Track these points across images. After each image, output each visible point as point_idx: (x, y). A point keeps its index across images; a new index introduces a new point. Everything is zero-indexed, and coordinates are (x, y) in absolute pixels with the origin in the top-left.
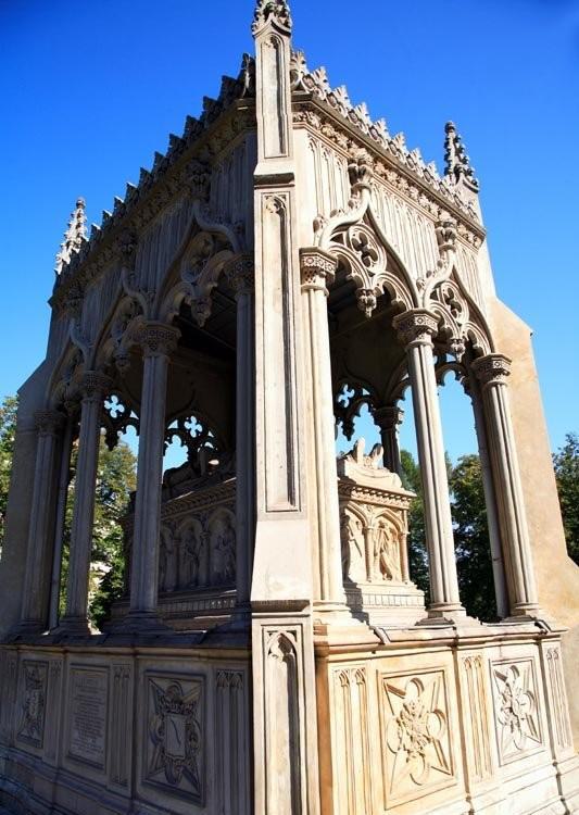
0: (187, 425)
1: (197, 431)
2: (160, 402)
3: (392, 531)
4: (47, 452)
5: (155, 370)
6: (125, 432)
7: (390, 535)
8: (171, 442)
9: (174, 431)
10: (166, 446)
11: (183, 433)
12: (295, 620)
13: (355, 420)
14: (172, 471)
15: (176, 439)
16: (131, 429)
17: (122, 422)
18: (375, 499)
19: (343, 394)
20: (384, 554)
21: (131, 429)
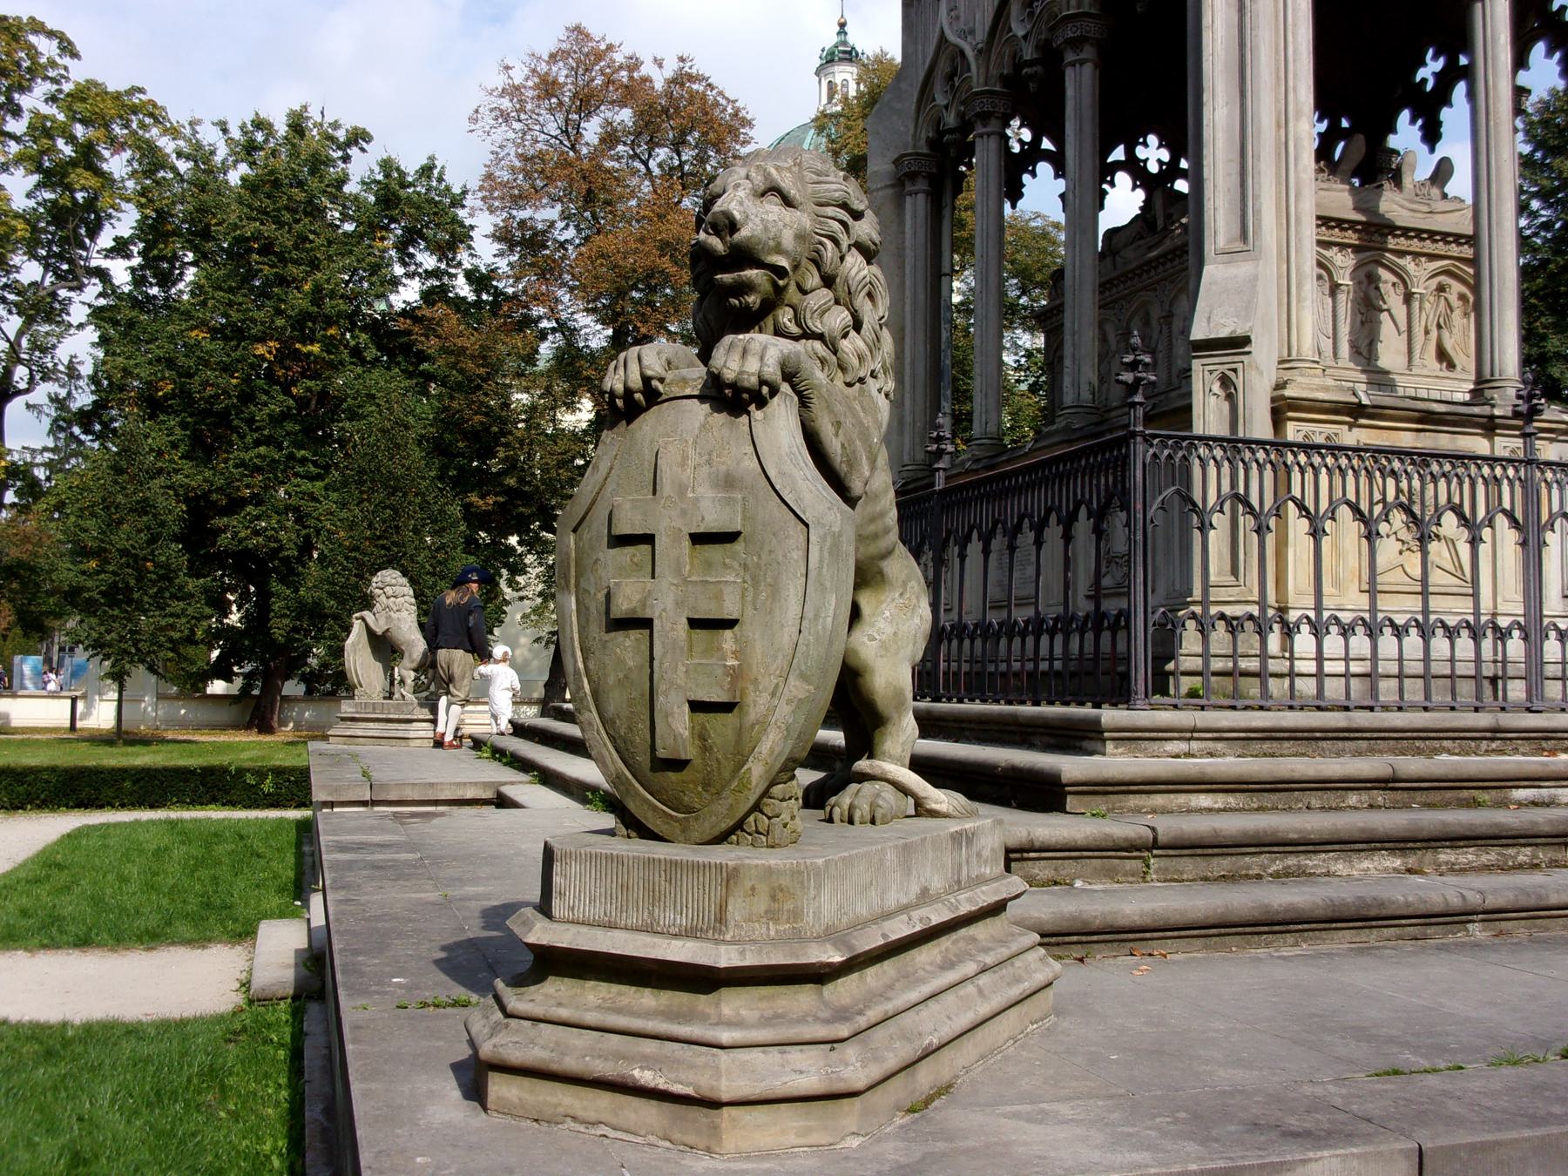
0: (1140, 152)
1: (1159, 161)
2: (1090, 129)
3: (1462, 297)
4: (921, 213)
5: (1080, 86)
6: (1034, 174)
7: (1455, 303)
8: (1112, 184)
9: (1118, 166)
10: (1104, 193)
11: (1135, 168)
12: (1236, 358)
13: (1445, 114)
14: (1112, 233)
15: (1123, 179)
16: (1044, 168)
17: (1032, 155)
18: (1429, 247)
19: (1434, 74)
20: (1445, 334)
21: (1044, 168)
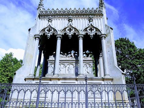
18: (67, 62)
